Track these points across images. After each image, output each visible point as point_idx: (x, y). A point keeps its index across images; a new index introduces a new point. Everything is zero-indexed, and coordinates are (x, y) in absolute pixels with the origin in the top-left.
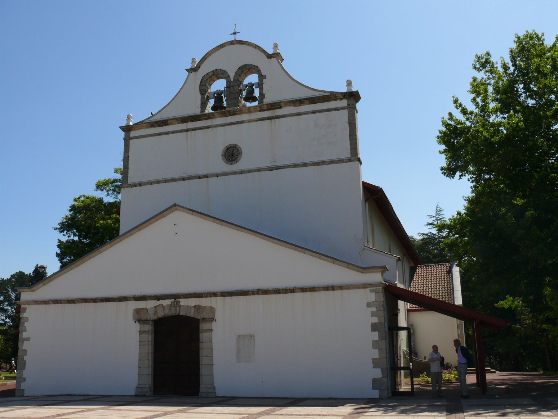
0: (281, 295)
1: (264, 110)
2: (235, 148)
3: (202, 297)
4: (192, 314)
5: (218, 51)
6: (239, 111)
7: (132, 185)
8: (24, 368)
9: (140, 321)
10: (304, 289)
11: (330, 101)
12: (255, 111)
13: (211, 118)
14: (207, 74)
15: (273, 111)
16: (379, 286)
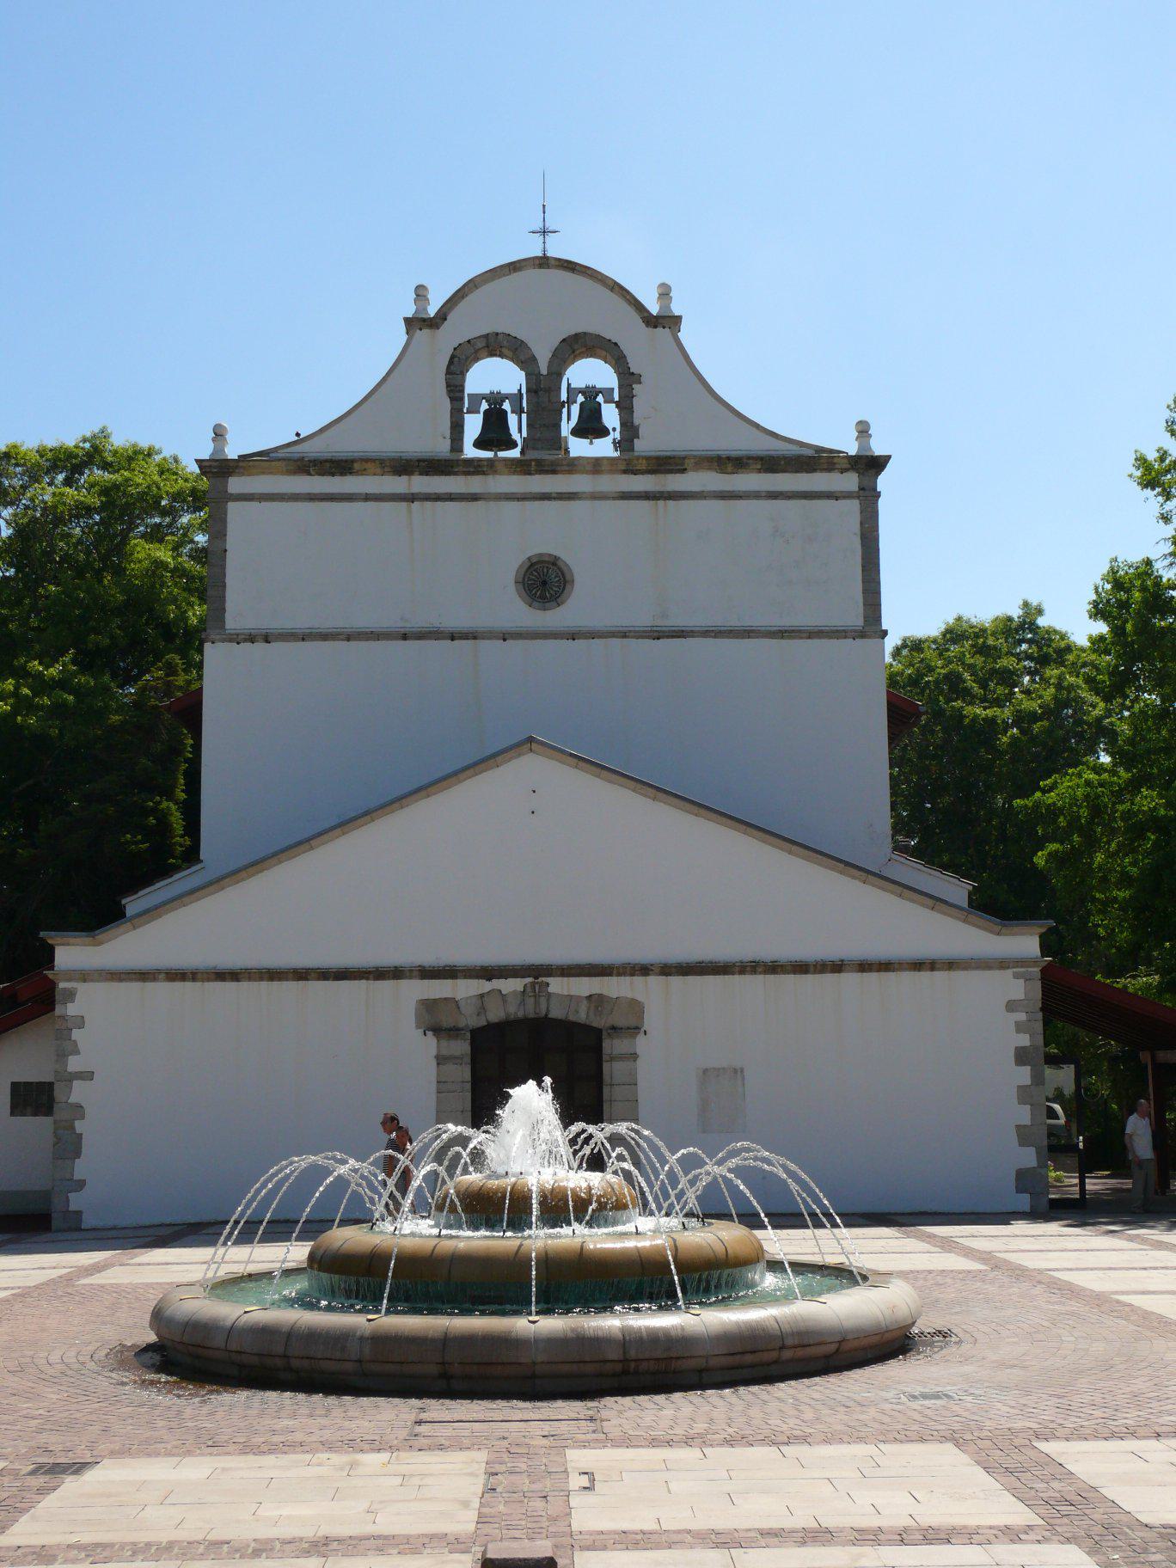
0: (809, 977)
1: (635, 472)
2: (550, 566)
3: (610, 974)
4: (582, 1015)
5: (499, 278)
6: (568, 465)
7: (243, 637)
8: (78, 1154)
9: (438, 1028)
10: (867, 966)
11: (814, 471)
12: (612, 472)
13: (484, 473)
14: (469, 341)
15: (661, 477)
16: (1034, 967)
